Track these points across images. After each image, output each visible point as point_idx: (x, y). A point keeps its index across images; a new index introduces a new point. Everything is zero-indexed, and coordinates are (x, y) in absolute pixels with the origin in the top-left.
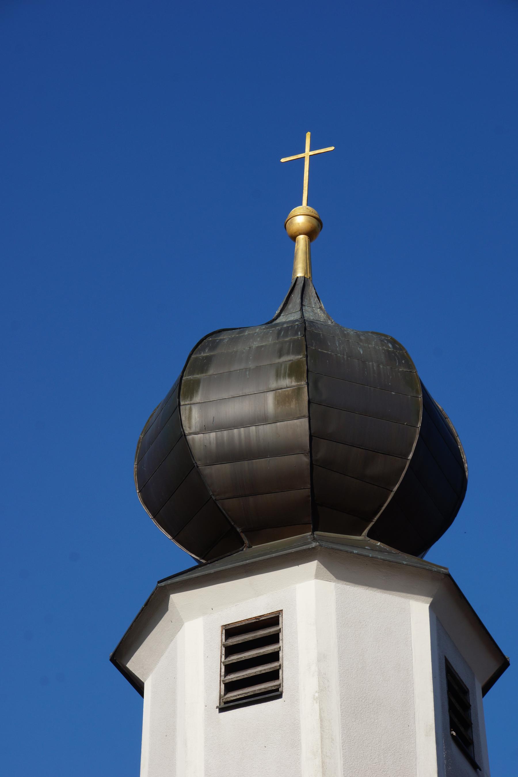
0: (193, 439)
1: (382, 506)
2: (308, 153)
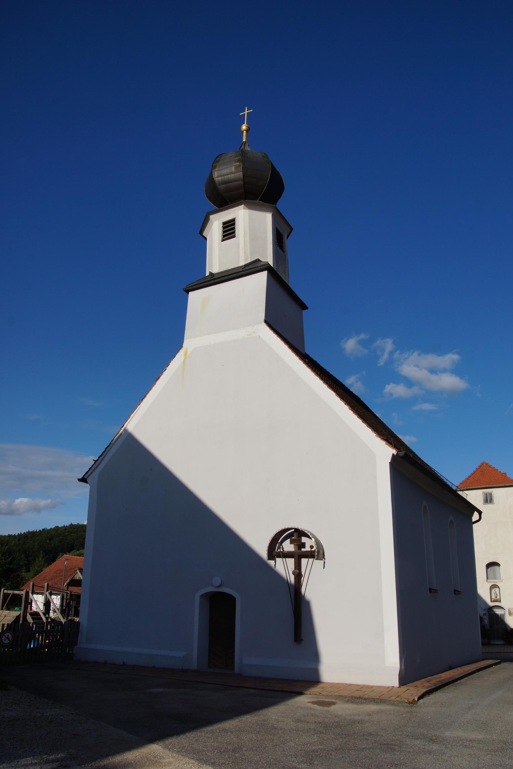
0: (215, 179)
1: (262, 193)
2: (246, 112)
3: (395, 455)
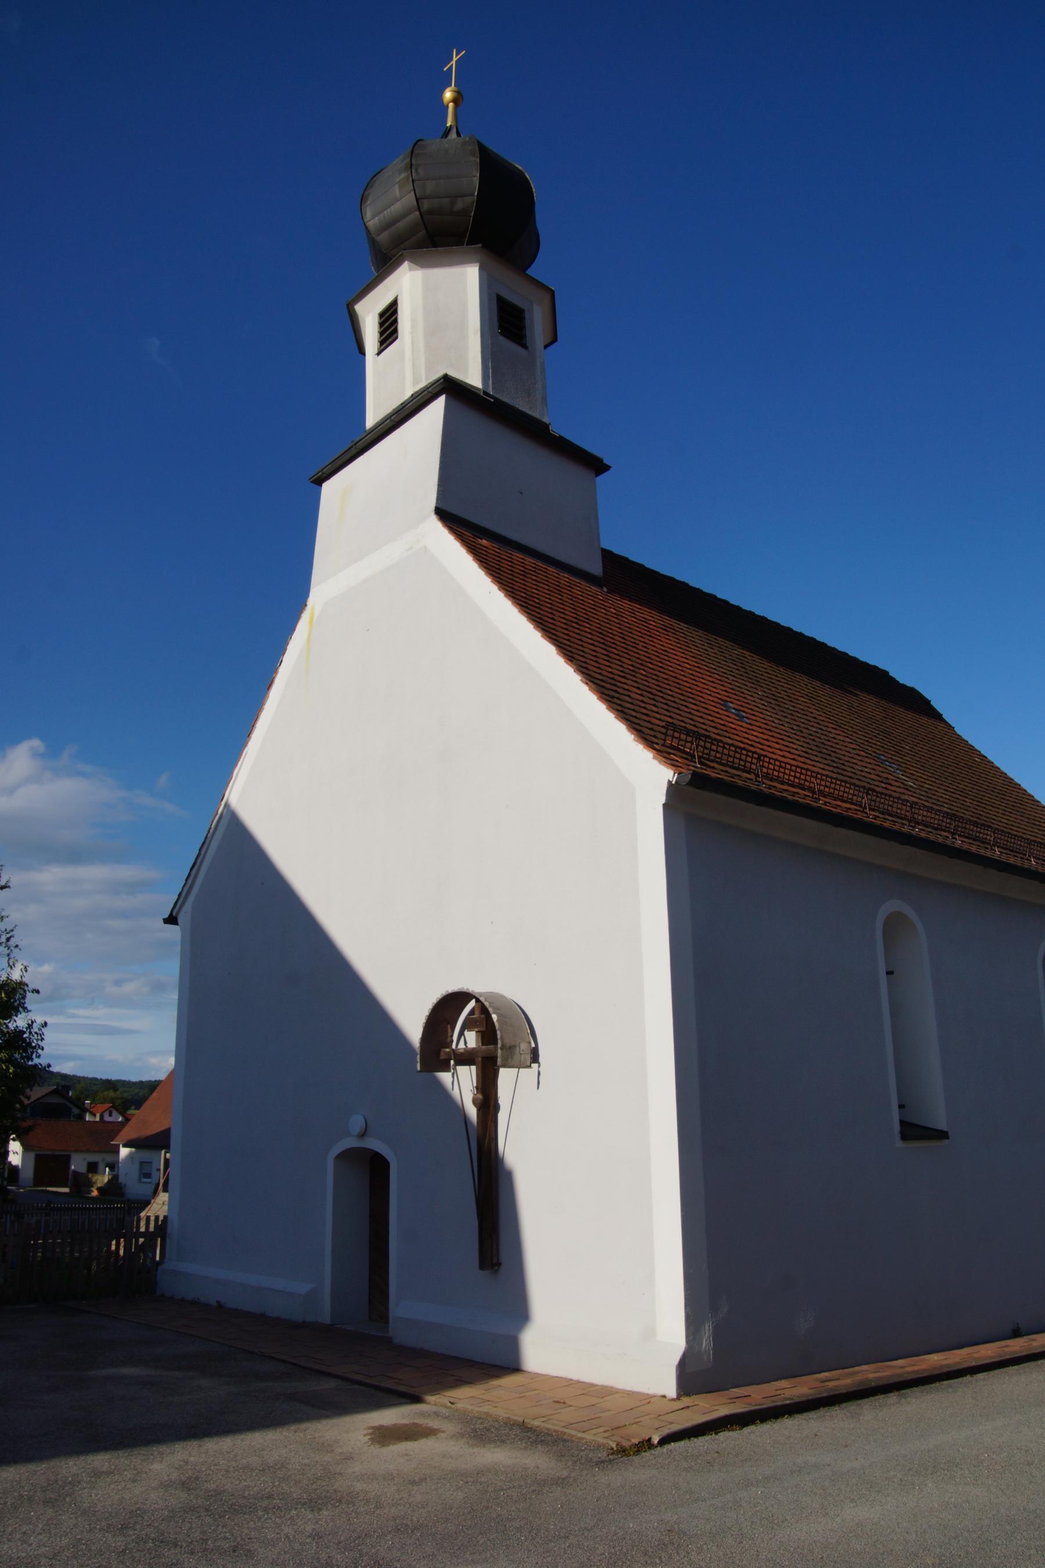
3: (674, 783)
